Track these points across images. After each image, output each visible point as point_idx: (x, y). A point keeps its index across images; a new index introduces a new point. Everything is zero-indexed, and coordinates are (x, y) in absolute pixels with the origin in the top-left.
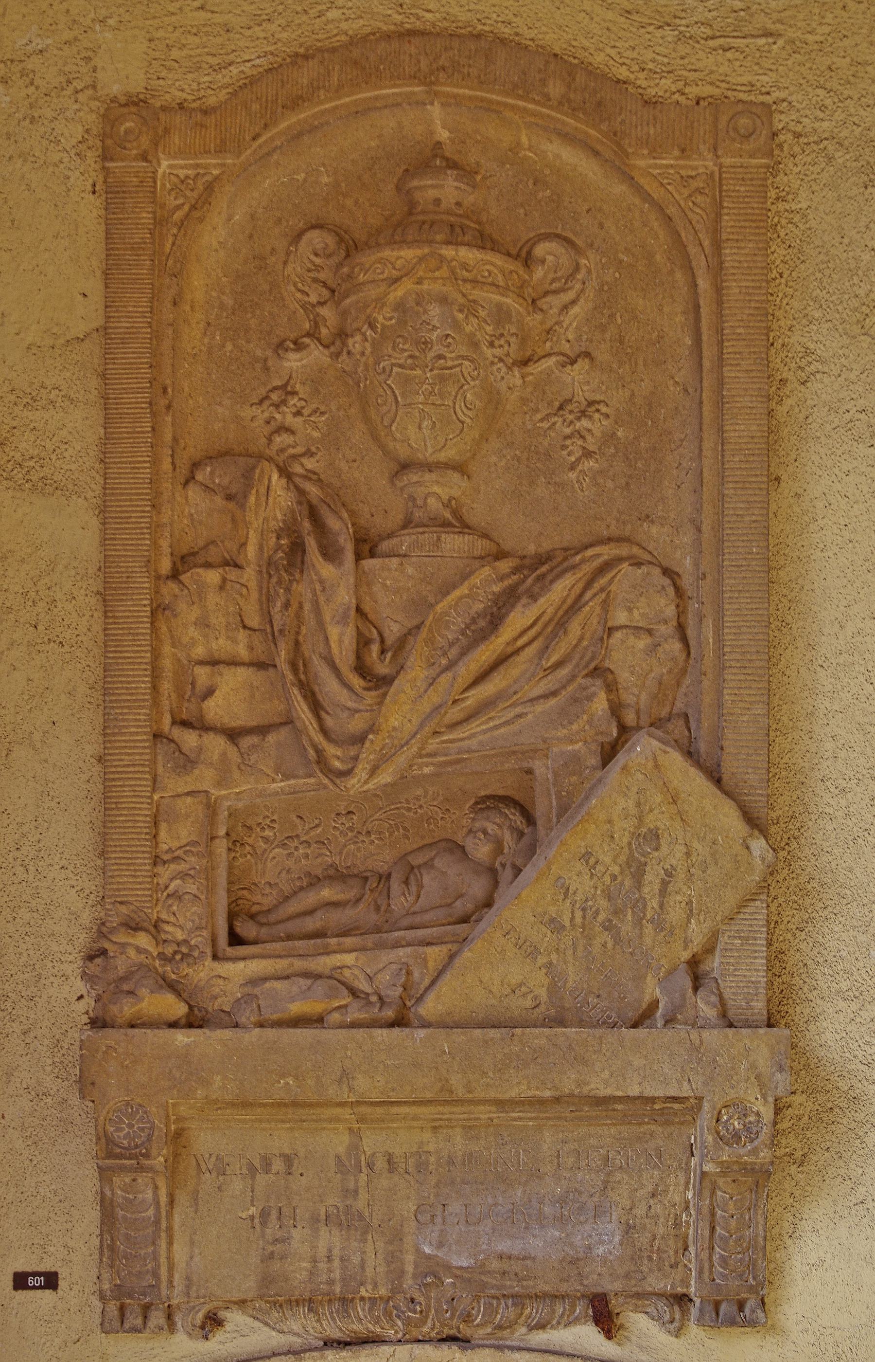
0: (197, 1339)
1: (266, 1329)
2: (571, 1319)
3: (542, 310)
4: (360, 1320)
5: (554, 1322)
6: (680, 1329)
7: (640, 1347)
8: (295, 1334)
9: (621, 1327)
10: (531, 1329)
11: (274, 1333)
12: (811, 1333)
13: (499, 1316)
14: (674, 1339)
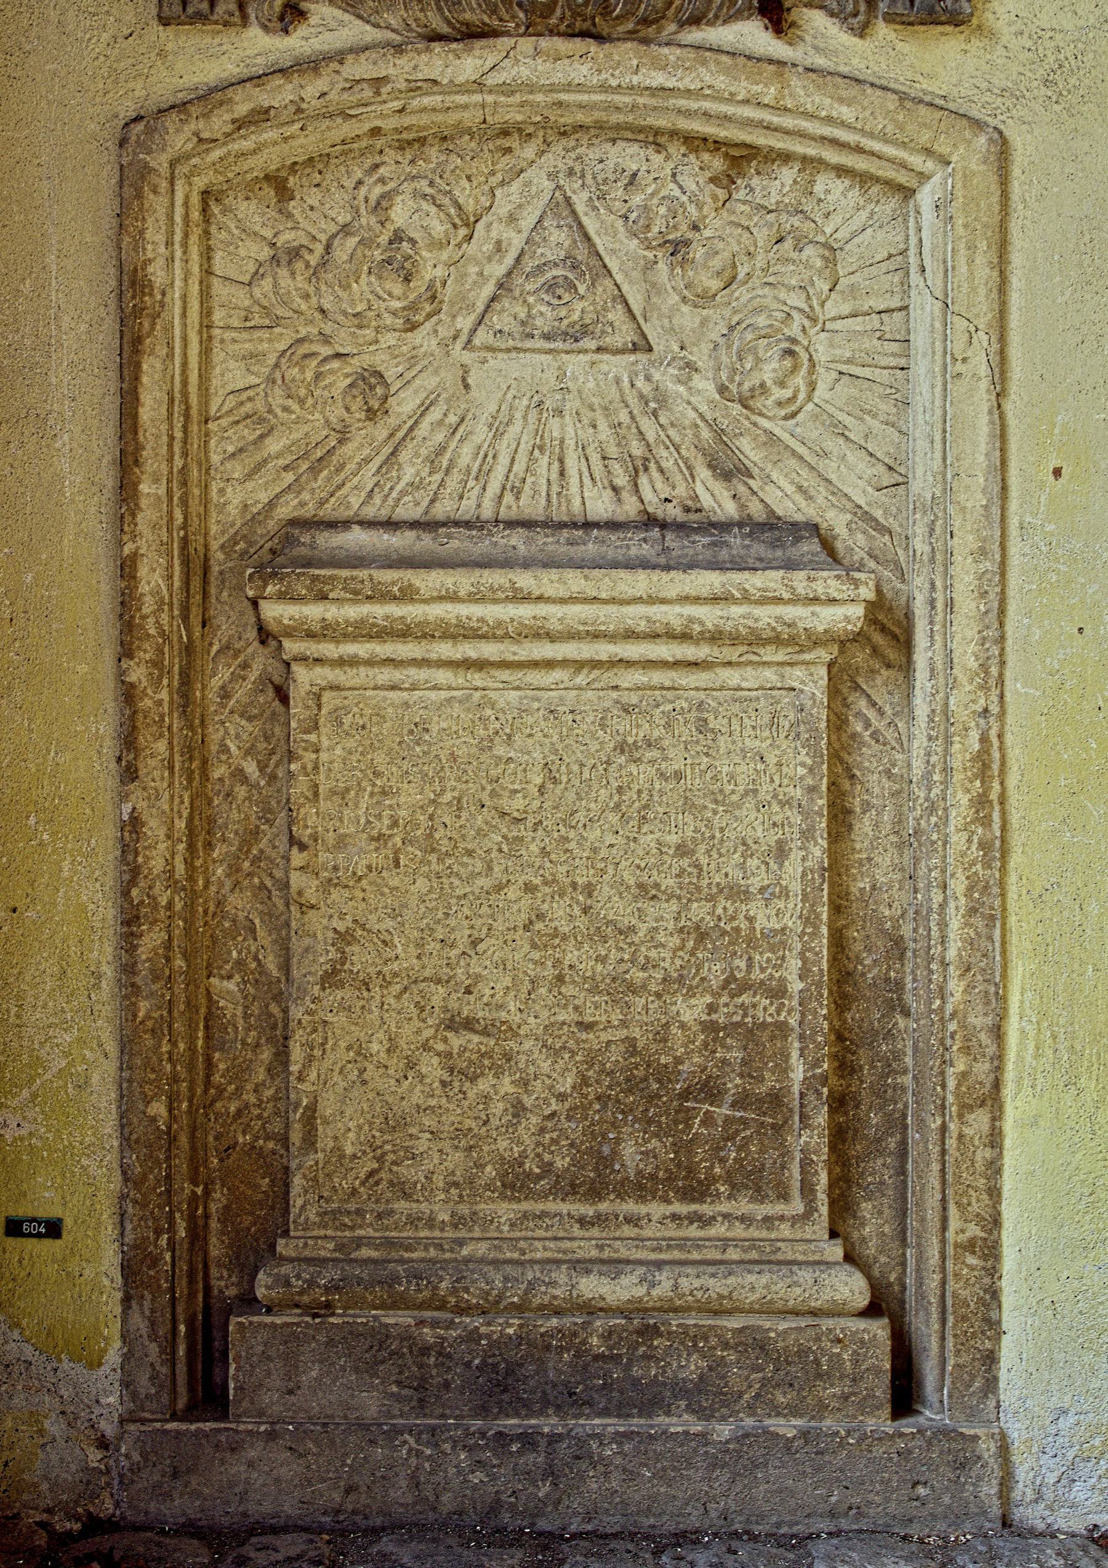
0: (275, 32)
1: (359, 22)
2: (731, 12)
3: (312, 907)
4: (472, 10)
5: (711, 15)
6: (866, 25)
7: (816, 48)
8: (393, 30)
9: (793, 24)
10: (682, 25)
11: (368, 28)
12: (1026, 35)
13: (643, 6)
14: (856, 40)
